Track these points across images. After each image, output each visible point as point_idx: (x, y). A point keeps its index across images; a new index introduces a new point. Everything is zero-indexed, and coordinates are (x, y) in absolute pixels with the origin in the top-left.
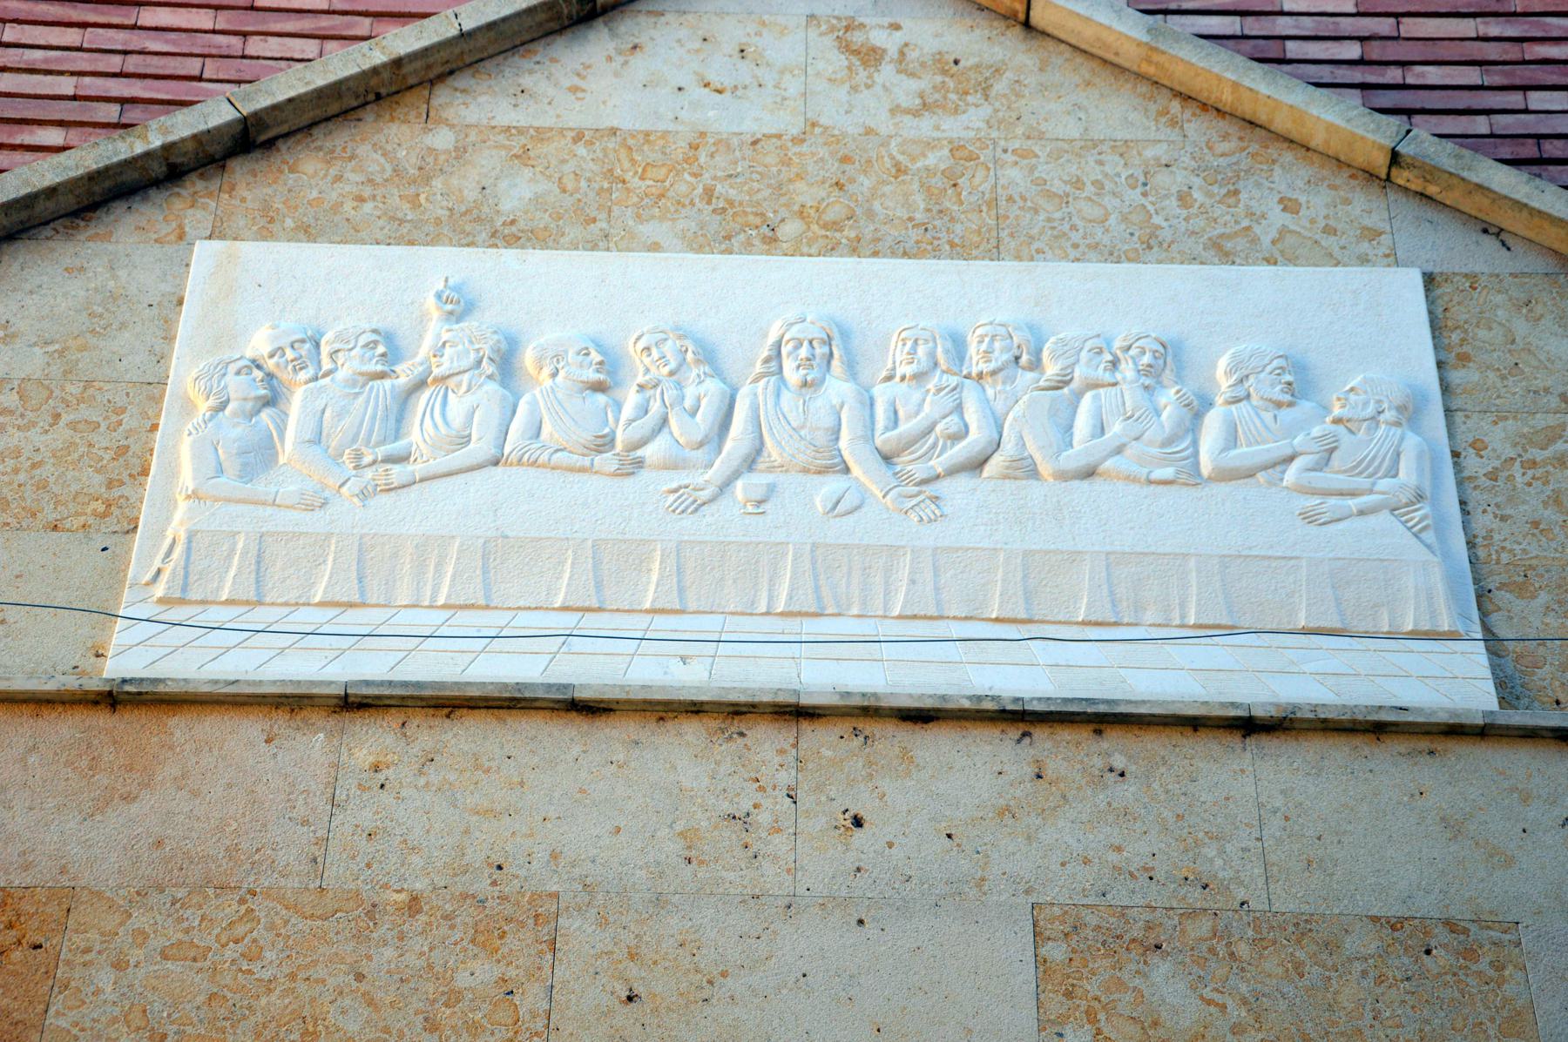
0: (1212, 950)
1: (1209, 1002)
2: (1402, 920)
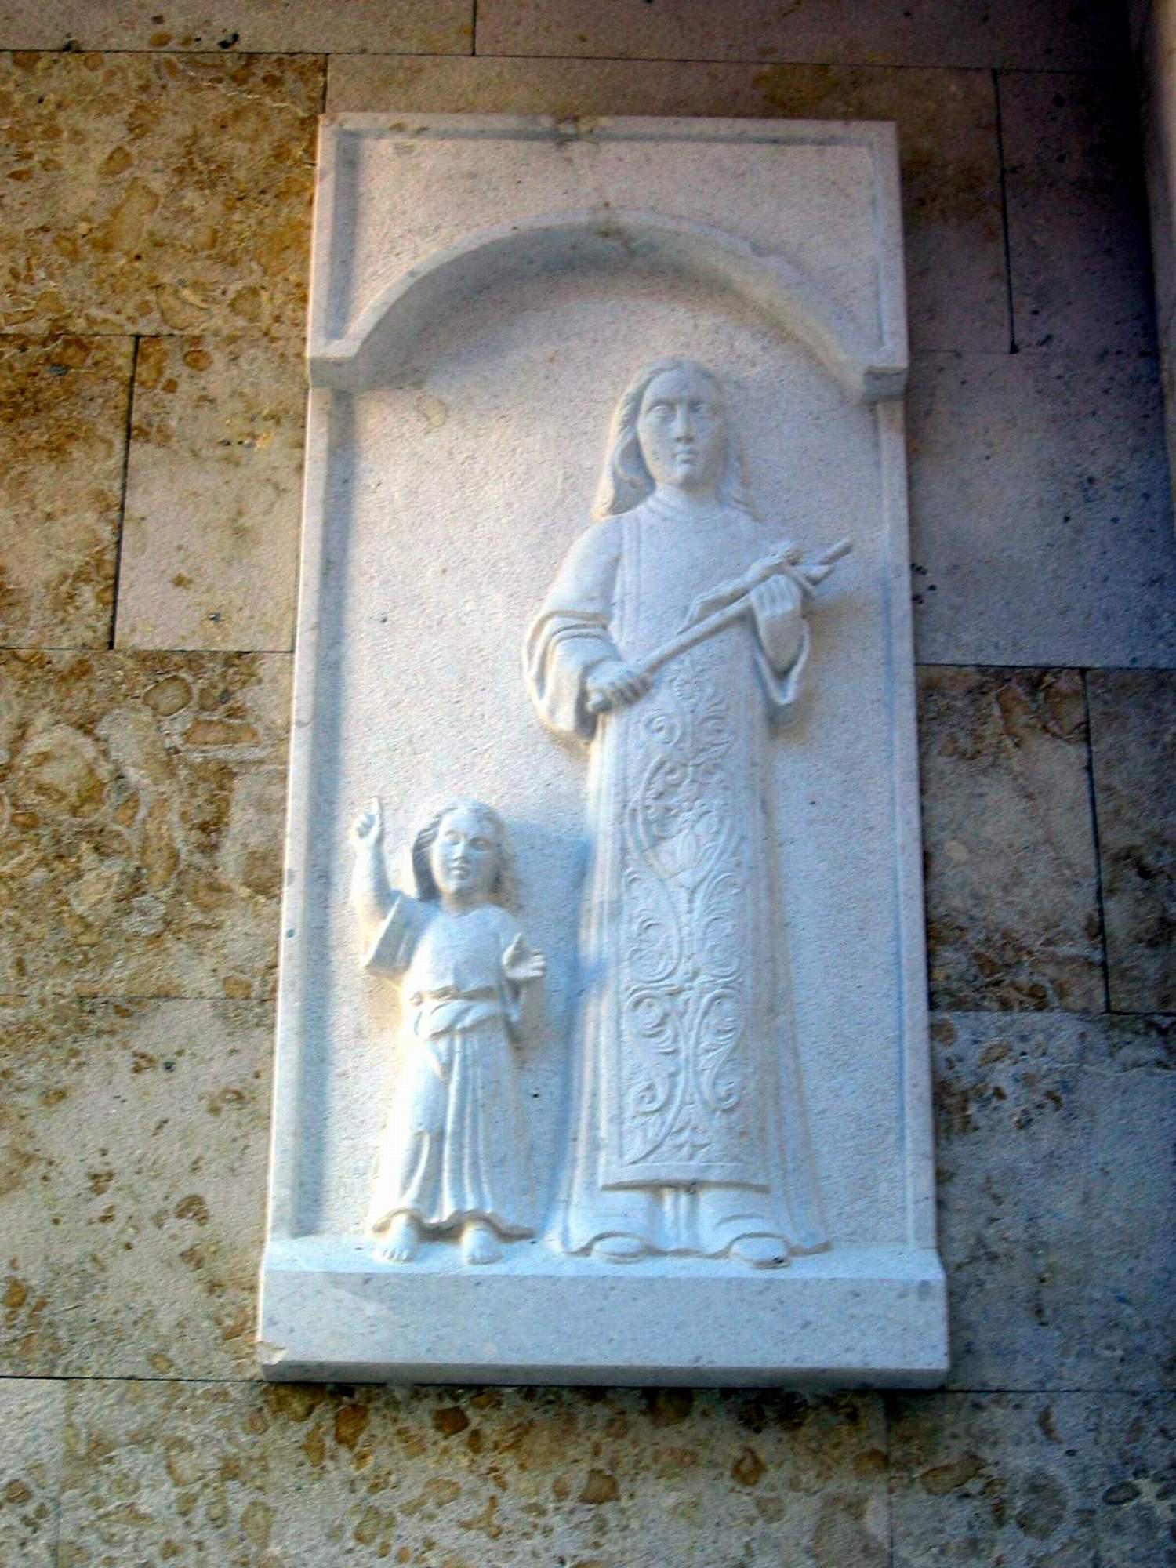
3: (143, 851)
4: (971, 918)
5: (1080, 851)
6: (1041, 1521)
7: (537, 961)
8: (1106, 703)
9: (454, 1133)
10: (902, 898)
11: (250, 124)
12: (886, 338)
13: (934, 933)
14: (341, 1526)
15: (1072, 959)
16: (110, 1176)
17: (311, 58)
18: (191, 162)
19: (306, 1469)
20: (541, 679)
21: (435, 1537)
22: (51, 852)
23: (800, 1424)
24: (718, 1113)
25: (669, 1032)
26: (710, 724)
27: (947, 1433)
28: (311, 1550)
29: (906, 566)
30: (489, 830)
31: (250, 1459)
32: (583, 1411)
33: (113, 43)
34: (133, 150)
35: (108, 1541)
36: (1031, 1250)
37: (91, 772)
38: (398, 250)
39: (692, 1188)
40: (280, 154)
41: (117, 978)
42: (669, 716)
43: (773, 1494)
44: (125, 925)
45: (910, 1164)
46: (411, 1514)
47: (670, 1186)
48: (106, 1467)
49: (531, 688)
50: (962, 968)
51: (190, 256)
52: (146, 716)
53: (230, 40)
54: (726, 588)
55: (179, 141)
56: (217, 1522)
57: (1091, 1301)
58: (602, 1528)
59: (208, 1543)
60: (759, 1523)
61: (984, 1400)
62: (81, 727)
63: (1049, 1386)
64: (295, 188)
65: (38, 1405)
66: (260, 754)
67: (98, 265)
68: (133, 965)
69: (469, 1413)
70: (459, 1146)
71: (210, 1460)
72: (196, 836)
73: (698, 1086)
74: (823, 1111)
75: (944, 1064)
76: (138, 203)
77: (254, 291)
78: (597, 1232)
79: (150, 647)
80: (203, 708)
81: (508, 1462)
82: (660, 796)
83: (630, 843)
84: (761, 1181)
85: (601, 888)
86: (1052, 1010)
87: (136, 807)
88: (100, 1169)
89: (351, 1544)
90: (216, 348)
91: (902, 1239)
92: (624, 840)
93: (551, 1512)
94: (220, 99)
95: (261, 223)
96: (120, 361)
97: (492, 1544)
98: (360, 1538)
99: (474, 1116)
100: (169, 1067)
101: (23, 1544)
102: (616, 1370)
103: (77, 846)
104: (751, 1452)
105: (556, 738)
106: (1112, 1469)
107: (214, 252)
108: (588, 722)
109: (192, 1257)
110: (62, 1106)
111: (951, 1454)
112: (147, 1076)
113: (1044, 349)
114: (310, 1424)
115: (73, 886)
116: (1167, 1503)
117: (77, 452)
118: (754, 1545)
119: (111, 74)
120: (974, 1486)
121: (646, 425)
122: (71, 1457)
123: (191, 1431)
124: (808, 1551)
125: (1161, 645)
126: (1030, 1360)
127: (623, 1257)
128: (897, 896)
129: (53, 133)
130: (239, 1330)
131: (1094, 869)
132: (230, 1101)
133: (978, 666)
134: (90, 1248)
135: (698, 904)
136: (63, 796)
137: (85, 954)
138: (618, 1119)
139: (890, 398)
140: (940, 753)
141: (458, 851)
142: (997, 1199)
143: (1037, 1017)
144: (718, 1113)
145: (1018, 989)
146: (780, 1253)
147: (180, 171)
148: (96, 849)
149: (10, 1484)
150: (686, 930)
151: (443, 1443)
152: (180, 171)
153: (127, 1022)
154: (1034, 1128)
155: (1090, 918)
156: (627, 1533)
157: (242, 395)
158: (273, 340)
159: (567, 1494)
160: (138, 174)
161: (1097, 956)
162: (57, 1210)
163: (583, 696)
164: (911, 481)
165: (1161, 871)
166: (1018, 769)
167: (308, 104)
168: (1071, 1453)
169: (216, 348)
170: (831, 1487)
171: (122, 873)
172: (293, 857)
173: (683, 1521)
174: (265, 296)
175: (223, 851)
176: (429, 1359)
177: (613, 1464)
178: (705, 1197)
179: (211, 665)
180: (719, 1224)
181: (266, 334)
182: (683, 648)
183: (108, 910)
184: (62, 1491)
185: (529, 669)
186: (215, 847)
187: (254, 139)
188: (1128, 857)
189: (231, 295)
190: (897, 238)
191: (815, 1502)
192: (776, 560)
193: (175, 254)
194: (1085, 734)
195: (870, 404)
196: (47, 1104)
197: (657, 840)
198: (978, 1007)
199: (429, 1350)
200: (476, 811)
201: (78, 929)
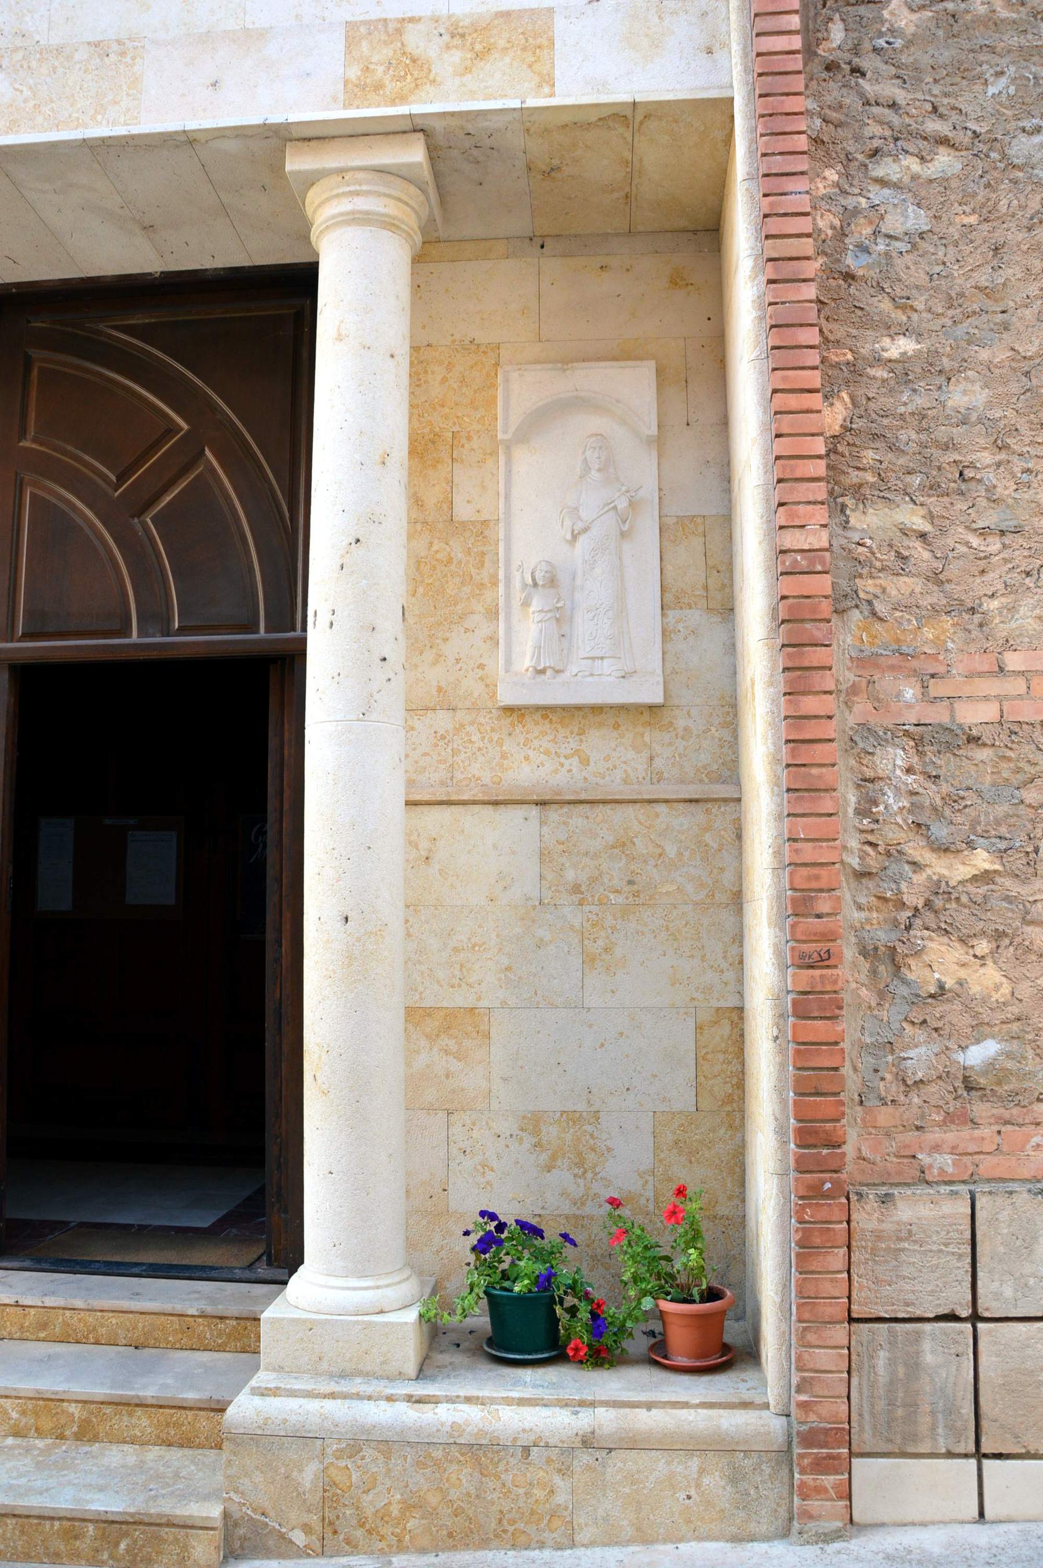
0: (22, 66)
1: (16, 90)
2: (99, 42)
32: (576, 713)
40: (488, 375)
52: (462, 539)
58: (581, 741)
81: (559, 726)
105: (567, 541)
109: (481, 679)
117: (439, 466)
120: (671, 729)
122: (455, 728)
123: (482, 720)
129: (426, 372)
130: (494, 695)
163: (573, 531)
178: (605, 660)
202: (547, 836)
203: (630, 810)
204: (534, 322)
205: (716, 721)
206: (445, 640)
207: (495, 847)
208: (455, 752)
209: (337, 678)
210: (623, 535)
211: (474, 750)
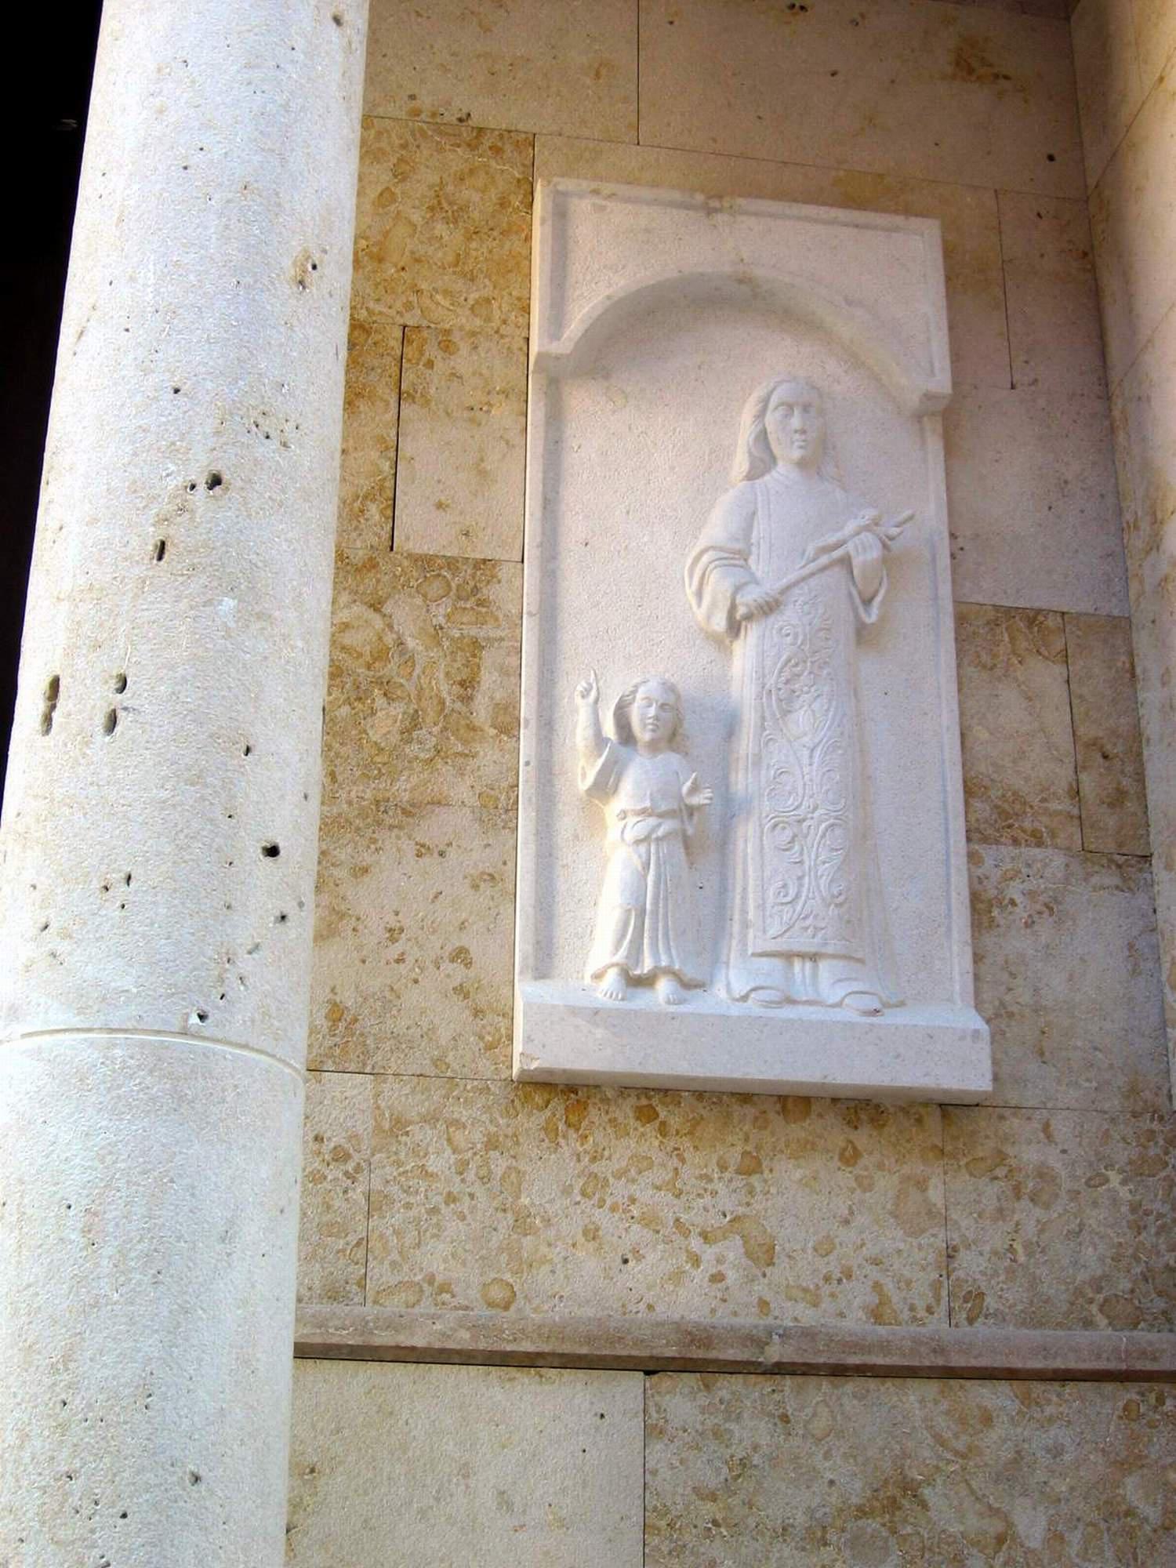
3: (419, 698)
4: (992, 780)
5: (1064, 741)
6: (1045, 1197)
7: (708, 793)
8: (1078, 637)
9: (652, 912)
10: (947, 764)
11: (480, 180)
12: (937, 371)
13: (970, 790)
14: (571, 1185)
15: (1058, 813)
16: (402, 930)
17: (523, 136)
18: (439, 203)
19: (545, 1145)
20: (699, 594)
21: (638, 1195)
22: (353, 697)
23: (884, 1125)
24: (832, 906)
25: (797, 848)
26: (821, 634)
27: (982, 1134)
28: (551, 1201)
29: (946, 534)
30: (672, 700)
31: (506, 1136)
32: (737, 1110)
33: (380, 111)
34: (397, 191)
35: (407, 1191)
36: (1036, 1011)
37: (380, 638)
38: (596, 280)
39: (814, 957)
41: (403, 788)
42: (794, 626)
43: (866, 1173)
44: (407, 751)
45: (955, 948)
46: (620, 1178)
47: (798, 956)
48: (404, 1138)
49: (693, 601)
50: (987, 814)
51: (441, 270)
52: (419, 601)
53: (464, 117)
54: (832, 539)
55: (430, 187)
56: (484, 1179)
57: (1076, 1048)
58: (751, 1192)
59: (478, 1194)
60: (858, 1191)
61: (1007, 1113)
62: (371, 606)
63: (1049, 1105)
64: (515, 228)
65: (355, 1092)
66: (499, 633)
67: (375, 272)
68: (414, 780)
69: (658, 1109)
70: (655, 922)
71: (478, 1137)
72: (456, 689)
73: (818, 886)
74: (896, 909)
75: (976, 880)
76: (402, 230)
77: (488, 301)
78: (753, 985)
79: (420, 552)
80: (459, 598)
81: (686, 1143)
82: (787, 682)
83: (767, 714)
84: (859, 955)
85: (746, 743)
86: (1046, 847)
87: (414, 665)
88: (393, 924)
89: (578, 1198)
90: (462, 339)
91: (950, 1000)
92: (763, 712)
93: (716, 1181)
94: (458, 159)
95: (490, 252)
96: (392, 343)
97: (676, 1201)
98: (583, 1194)
99: (666, 899)
100: (442, 854)
101: (345, 1192)
102: (763, 1082)
103: (372, 692)
104: (851, 1142)
106: (1091, 1164)
107: (458, 269)
108: (734, 627)
109: (461, 991)
110: (366, 879)
111: (985, 1149)
112: (427, 860)
113: (1033, 388)
114: (548, 1113)
115: (369, 720)
116: (1126, 1188)
118: (854, 1207)
119: (379, 134)
120: (1000, 1172)
121: (771, 420)
123: (463, 1114)
124: (891, 1213)
125: (1114, 600)
126: (1037, 1087)
127: (769, 1004)
128: (943, 762)
131: (1073, 751)
132: (485, 880)
133: (994, 606)
134: (389, 982)
135: (816, 760)
136: (360, 655)
137: (380, 770)
138: (762, 907)
139: (933, 414)
140: (969, 665)
141: (652, 712)
142: (1013, 975)
143: (1037, 851)
144: (832, 906)
145: (1024, 831)
146: (877, 1006)
147: (431, 209)
148: (385, 695)
149: (335, 1148)
150: (807, 777)
151: (642, 1130)
152: (431, 209)
153: (410, 820)
154: (1036, 927)
155: (1070, 785)
156: (769, 1196)
157: (481, 374)
158: (502, 337)
159: (726, 1169)
160: (401, 208)
161: (1075, 812)
162: (365, 953)
164: (948, 472)
165: (1117, 756)
166: (1021, 679)
167: (522, 169)
168: (1064, 1151)
169: (462, 339)
170: (906, 1169)
171: (404, 713)
172: (527, 708)
173: (807, 1190)
174: (495, 304)
175: (476, 702)
176: (639, 1070)
177: (758, 1148)
178: (824, 965)
179: (465, 567)
180: (834, 983)
181: (497, 332)
182: (804, 579)
183: (395, 738)
184: (373, 1155)
185: (690, 585)
186: (471, 698)
187: (484, 190)
188: (1094, 745)
189: (471, 302)
190: (942, 303)
191: (896, 1178)
192: (863, 522)
193: (430, 268)
194: (1065, 657)
195: (918, 417)
196: (356, 877)
197: (786, 713)
198: (997, 842)
199: (640, 1064)
200: (664, 684)
201: (374, 751)
202: (665, 1473)
203: (914, 1397)
204: (625, 100)
205: (1122, 1155)
206: (361, 871)
207: (504, 1501)
208: (374, 1204)
209: (120, 891)
210: (864, 635)
211: (437, 1200)
